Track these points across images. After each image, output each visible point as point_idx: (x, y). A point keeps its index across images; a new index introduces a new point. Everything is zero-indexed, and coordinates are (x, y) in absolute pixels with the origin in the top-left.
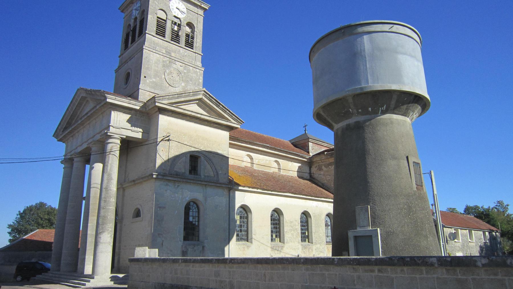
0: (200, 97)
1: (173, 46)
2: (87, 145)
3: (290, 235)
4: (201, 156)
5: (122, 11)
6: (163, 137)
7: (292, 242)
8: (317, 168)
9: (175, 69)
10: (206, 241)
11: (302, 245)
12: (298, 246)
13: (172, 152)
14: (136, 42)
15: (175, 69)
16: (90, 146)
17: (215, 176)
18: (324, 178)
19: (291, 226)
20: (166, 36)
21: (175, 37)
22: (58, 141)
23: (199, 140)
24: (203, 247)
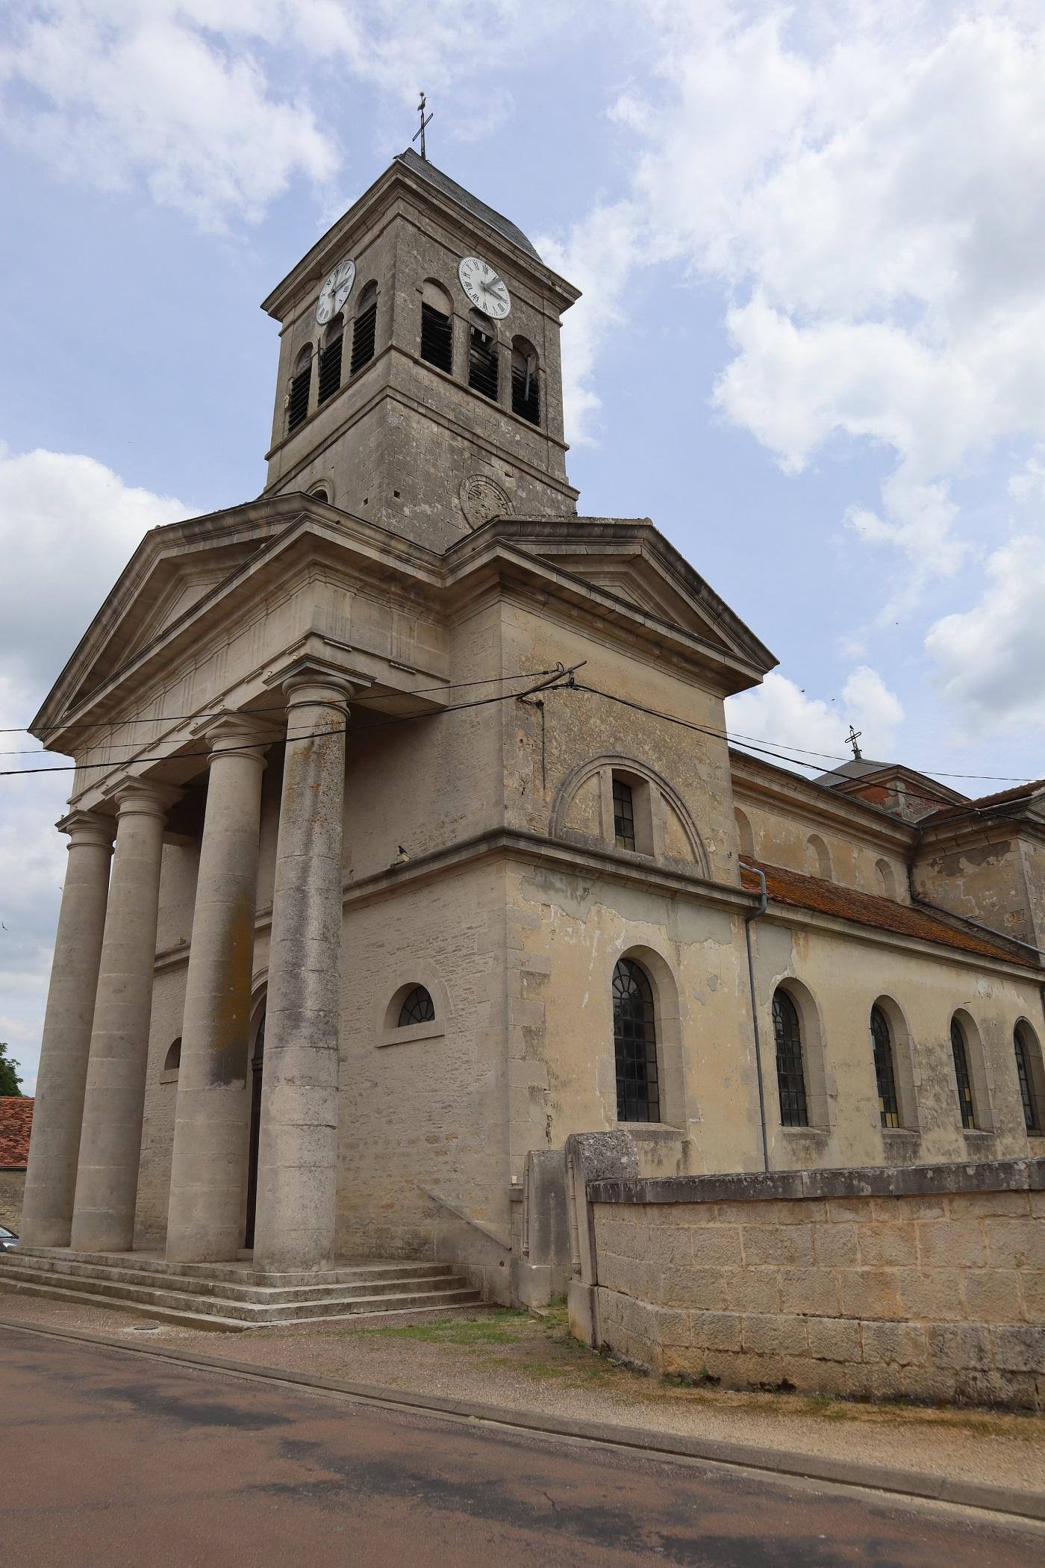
0: (634, 549)
1: (474, 408)
2: (104, 793)
3: (930, 1102)
4: (651, 781)
5: (274, 314)
6: (545, 673)
7: (938, 1126)
8: (937, 868)
9: (490, 482)
10: (691, 1120)
11: (967, 1138)
12: (957, 1141)
13: (554, 751)
14: (343, 392)
15: (490, 482)
16: (203, 738)
17: (697, 862)
18: (969, 900)
19: (930, 1065)
20: (454, 368)
21: (483, 380)
22: (49, 748)
23: (635, 715)
24: (686, 1145)
